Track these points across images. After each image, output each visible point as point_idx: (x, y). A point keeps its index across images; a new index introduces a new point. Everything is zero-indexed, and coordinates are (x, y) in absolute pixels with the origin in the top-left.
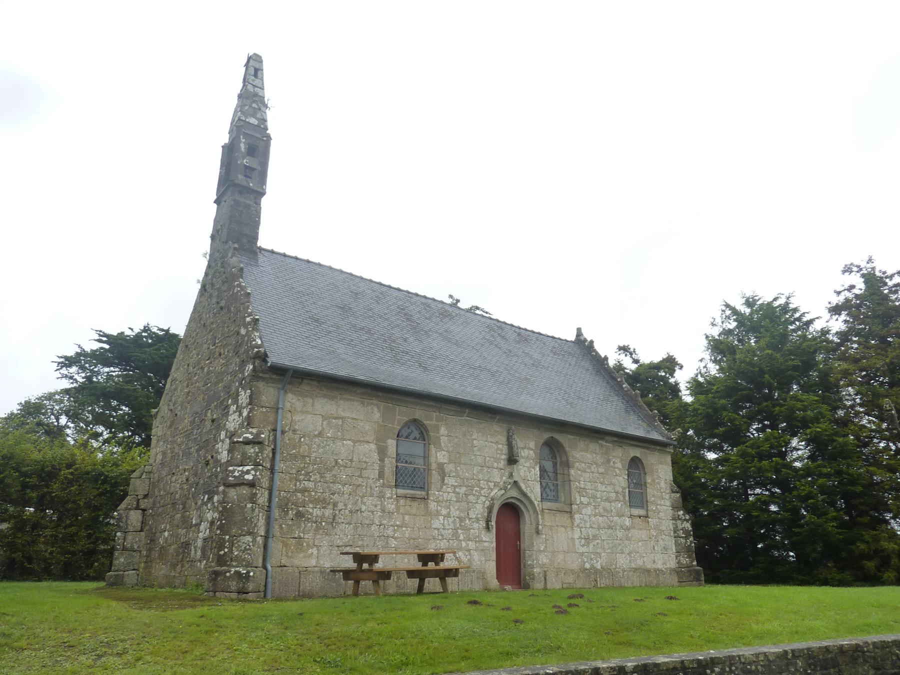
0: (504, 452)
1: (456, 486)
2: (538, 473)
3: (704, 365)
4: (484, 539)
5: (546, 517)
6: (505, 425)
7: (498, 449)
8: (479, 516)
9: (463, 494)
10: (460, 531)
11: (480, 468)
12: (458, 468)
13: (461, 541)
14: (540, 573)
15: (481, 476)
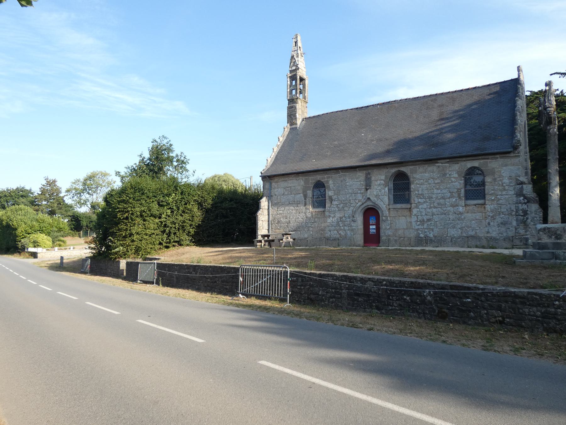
0: (364, 185)
2: (387, 191)
4: (353, 225)
5: (392, 212)
6: (365, 172)
10: (340, 223)
15: (351, 198)
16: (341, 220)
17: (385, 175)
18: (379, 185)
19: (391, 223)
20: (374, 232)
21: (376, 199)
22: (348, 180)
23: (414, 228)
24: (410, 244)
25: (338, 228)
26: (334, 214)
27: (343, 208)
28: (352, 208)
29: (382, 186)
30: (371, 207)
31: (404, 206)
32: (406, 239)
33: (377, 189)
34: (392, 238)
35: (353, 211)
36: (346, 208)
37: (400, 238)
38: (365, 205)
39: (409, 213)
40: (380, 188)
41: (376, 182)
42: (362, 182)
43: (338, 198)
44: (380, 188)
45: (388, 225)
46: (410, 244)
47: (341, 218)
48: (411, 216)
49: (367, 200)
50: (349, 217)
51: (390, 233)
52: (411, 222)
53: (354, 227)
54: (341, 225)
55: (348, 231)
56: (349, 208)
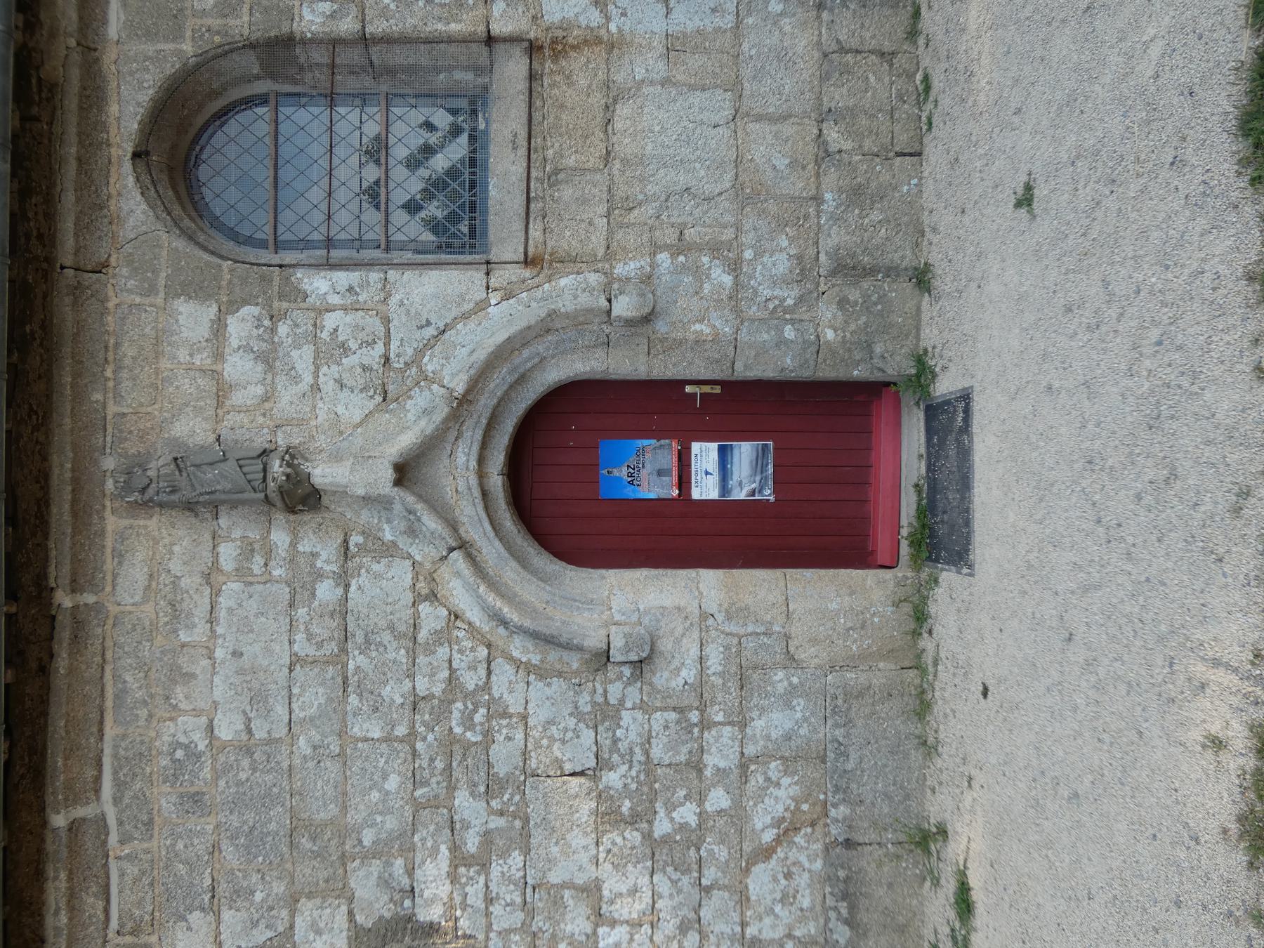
0: (254, 534)
1: (454, 848)
2: (343, 278)
3: (585, 844)
4: (689, 674)
5: (565, 240)
6: (113, 523)
7: (242, 573)
8: (584, 700)
9: (492, 812)
10: (662, 827)
11: (353, 700)
12: (368, 837)
13: (702, 815)
14: (843, 303)
15: (394, 692)
16: (633, 820)
17: (173, 292)
18: (268, 359)
19: (680, 247)
20: (758, 464)
21: (420, 400)
22: (189, 729)
23: (728, 21)
24: (887, 56)
25: (722, 853)
26: (557, 902)
27: (492, 787)
28: (504, 674)
29: (283, 329)
30: (498, 459)
31: (477, 257)
32: (838, 96)
33: (315, 388)
34: (834, 238)
35: (529, 668)
36: (504, 756)
37: (824, 154)
38: (476, 528)
39: (575, 63)
40: (302, 359)
41: (238, 398)
42: (228, 554)
43: (379, 852)
44: (308, 351)
45: (700, 274)
46: (887, 56)
47: (609, 816)
48: (613, 46)
49: (420, 497)
50: (606, 714)
51: (781, 264)
52: (674, 47)
53: (715, 662)
54: (687, 813)
55: (759, 724)
56: (498, 711)
